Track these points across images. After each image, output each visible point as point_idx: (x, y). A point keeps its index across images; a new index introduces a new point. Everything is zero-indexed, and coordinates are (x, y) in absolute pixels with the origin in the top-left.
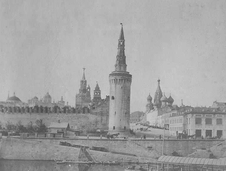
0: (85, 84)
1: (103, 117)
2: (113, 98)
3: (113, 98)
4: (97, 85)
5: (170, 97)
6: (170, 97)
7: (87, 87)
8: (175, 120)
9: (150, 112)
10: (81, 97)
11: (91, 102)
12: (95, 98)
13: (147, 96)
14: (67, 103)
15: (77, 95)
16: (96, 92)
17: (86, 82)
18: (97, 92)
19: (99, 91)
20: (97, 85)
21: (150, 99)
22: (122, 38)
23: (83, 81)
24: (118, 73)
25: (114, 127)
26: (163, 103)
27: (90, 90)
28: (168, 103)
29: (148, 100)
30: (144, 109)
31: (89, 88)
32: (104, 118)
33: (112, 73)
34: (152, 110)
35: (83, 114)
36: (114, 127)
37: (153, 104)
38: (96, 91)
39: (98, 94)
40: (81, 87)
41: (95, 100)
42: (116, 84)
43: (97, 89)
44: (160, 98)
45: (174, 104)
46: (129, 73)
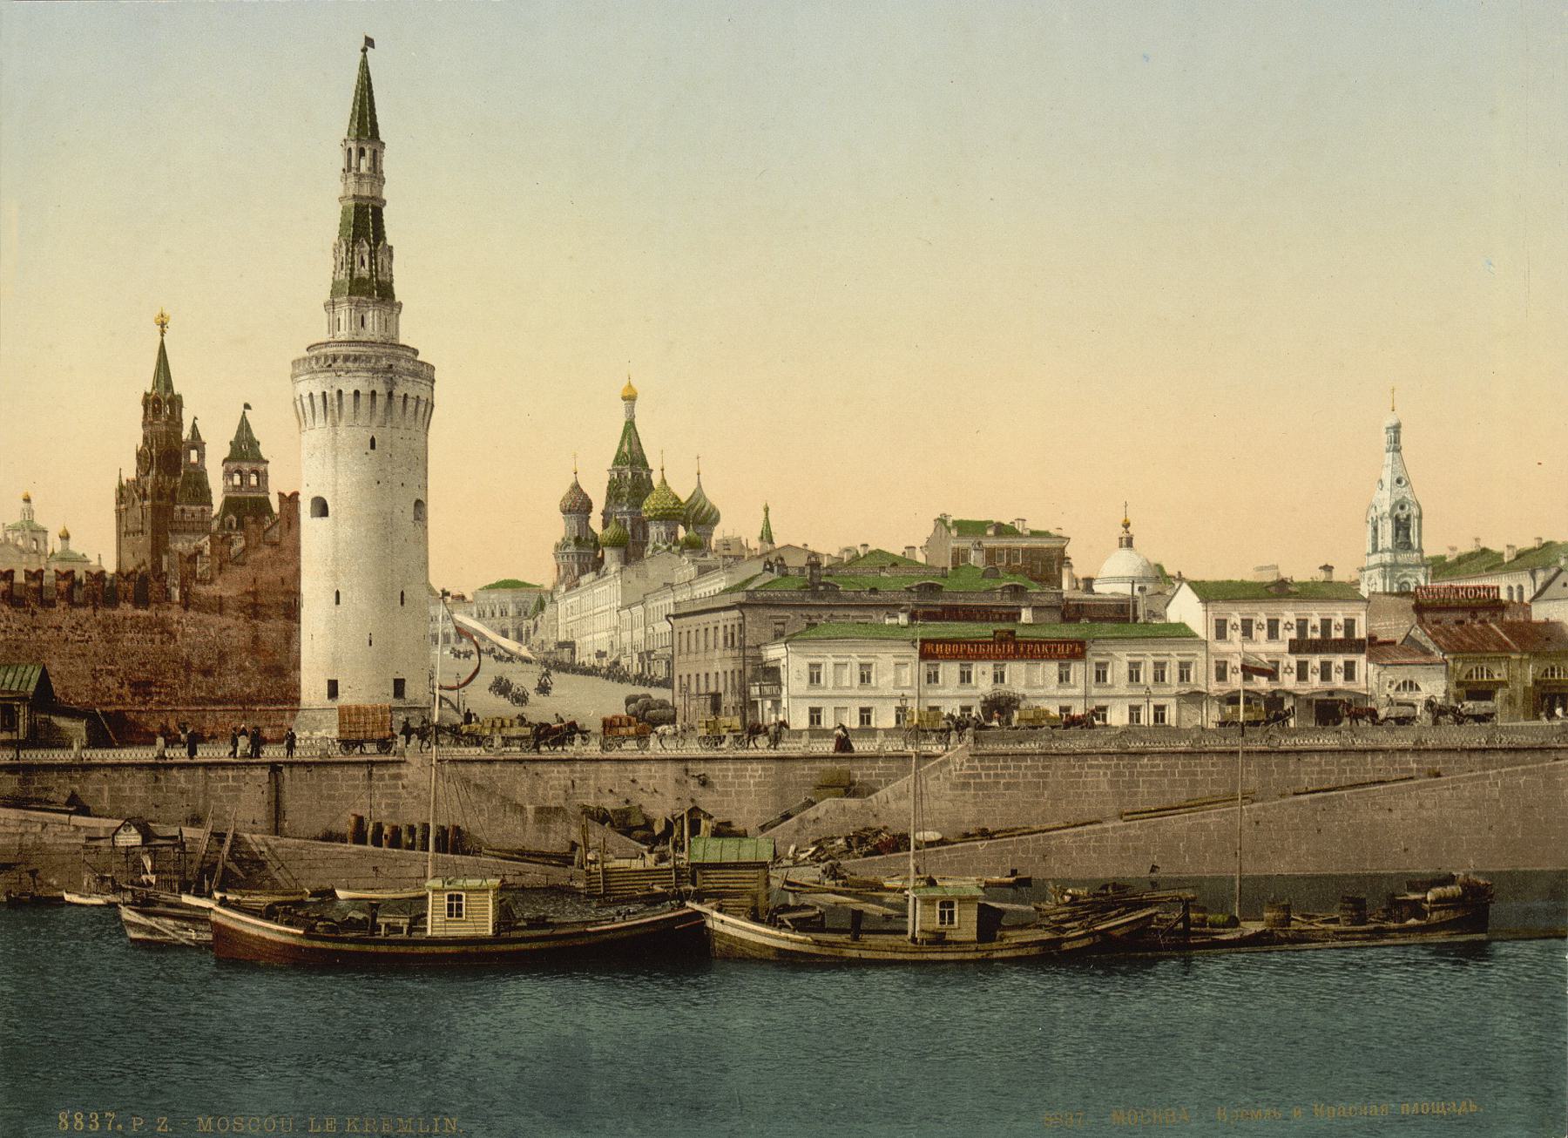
0: (175, 421)
1: (262, 625)
2: (321, 508)
3: (321, 508)
4: (244, 426)
5: (698, 494)
6: (698, 494)
7: (186, 434)
8: (685, 631)
9: (578, 586)
10: (147, 503)
11: (208, 533)
12: (229, 504)
13: (564, 489)
14: (65, 537)
15: (121, 487)
16: (239, 472)
17: (181, 406)
18: (246, 467)
19: (254, 466)
20: (244, 426)
21: (577, 506)
22: (365, 124)
23: (157, 400)
24: (345, 350)
25: (329, 681)
26: (655, 531)
27: (201, 456)
28: (687, 530)
29: (564, 512)
30: (542, 572)
31: (197, 443)
32: (270, 629)
33: (306, 354)
34: (590, 576)
35: (140, 612)
36: (329, 681)
37: (595, 536)
38: (233, 466)
39: (254, 480)
40: (145, 438)
41: (232, 517)
42: (334, 425)
43: (245, 450)
44: (639, 506)
45: (718, 534)
46: (416, 352)
